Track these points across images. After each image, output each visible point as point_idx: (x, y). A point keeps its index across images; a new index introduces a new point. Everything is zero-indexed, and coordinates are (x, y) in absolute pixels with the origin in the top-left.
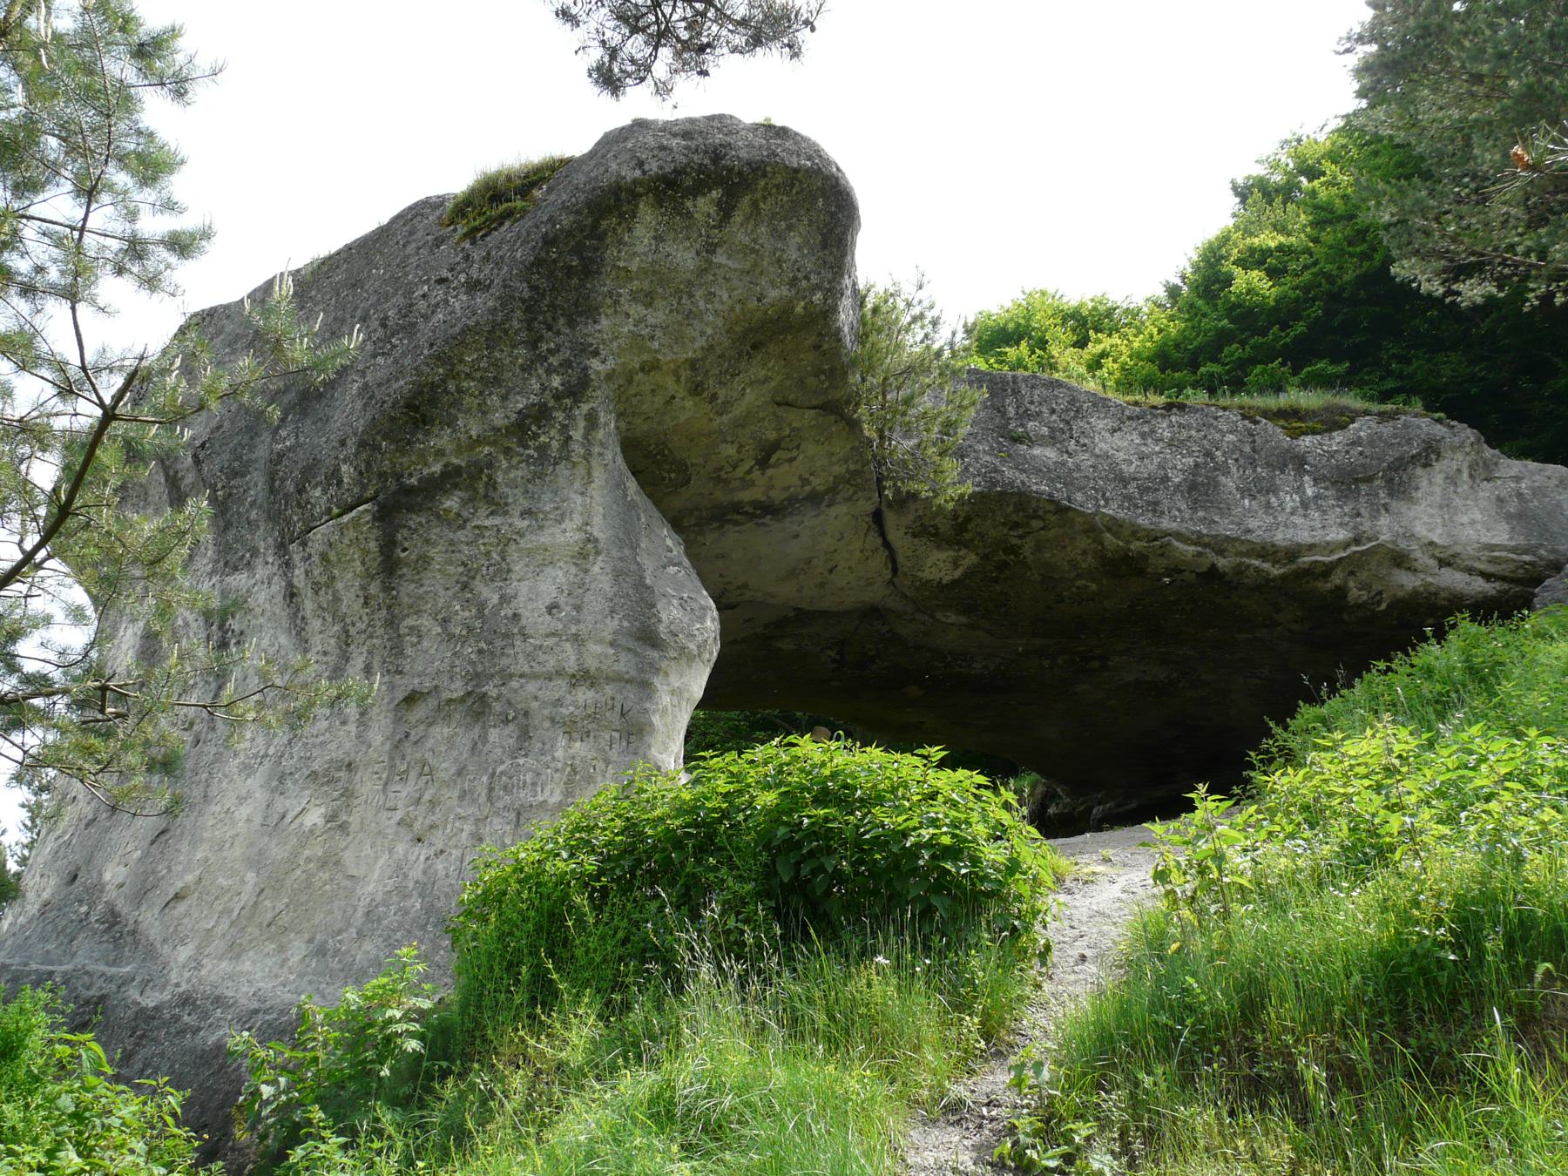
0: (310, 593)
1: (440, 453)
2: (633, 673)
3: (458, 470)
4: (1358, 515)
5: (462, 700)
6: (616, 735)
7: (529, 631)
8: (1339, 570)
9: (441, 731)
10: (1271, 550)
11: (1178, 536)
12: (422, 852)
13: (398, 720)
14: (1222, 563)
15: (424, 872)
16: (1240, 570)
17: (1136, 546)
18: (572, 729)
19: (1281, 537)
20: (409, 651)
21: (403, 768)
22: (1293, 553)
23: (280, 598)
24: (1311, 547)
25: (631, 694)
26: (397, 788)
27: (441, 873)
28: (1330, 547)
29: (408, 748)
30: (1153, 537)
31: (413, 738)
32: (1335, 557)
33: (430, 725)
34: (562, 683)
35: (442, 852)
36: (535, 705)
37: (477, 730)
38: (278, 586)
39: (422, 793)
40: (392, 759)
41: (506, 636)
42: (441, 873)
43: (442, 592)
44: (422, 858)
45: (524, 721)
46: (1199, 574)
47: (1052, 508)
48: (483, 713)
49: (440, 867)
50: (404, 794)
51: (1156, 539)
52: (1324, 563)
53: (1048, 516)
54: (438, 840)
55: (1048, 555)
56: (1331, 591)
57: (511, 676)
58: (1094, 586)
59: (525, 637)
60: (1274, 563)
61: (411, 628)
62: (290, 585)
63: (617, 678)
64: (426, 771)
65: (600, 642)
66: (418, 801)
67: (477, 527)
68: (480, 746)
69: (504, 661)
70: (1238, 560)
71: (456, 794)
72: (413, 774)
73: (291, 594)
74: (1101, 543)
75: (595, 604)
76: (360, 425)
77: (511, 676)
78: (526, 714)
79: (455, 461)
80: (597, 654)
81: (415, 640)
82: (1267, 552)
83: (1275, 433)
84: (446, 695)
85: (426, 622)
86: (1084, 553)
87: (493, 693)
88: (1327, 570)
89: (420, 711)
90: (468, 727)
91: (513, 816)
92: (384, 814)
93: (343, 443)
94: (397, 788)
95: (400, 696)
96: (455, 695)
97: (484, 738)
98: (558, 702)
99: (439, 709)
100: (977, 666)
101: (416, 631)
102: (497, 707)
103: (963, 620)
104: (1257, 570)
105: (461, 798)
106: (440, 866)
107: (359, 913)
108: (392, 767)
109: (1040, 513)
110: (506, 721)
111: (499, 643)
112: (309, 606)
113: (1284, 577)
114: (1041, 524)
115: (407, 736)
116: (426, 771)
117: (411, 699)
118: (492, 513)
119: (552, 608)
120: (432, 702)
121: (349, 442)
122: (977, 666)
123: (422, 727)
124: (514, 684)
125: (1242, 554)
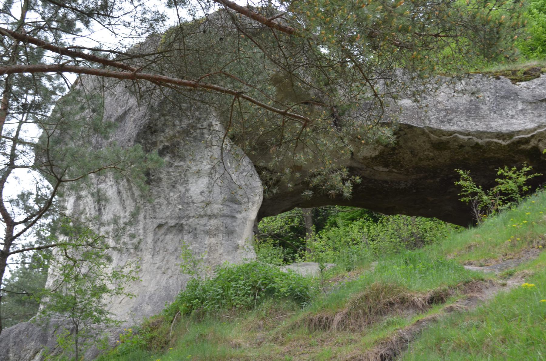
0: (125, 192)
1: (162, 142)
2: (229, 213)
3: (167, 147)
4: (540, 116)
5: (175, 226)
6: (224, 235)
7: (195, 201)
8: (533, 140)
9: (169, 237)
10: (501, 135)
11: (460, 133)
12: (166, 277)
13: (155, 234)
14: (480, 141)
15: (166, 283)
16: (489, 143)
17: (444, 138)
18: (208, 233)
19: (505, 129)
20: (157, 210)
21: (158, 250)
22: (511, 135)
23: (116, 193)
24: (519, 132)
25: (228, 221)
26: (156, 257)
27: (171, 283)
28: (526, 131)
29: (159, 243)
30: (451, 133)
31: (161, 240)
32: (529, 135)
33: (166, 235)
34: (206, 218)
35: (171, 277)
36: (198, 226)
37: (180, 236)
38: (115, 189)
39: (164, 257)
40: (154, 247)
41: (187, 203)
42: (171, 283)
43: (166, 189)
44: (165, 279)
45: (195, 232)
46: (472, 147)
47: (406, 127)
48: (182, 230)
49: (171, 281)
50: (158, 259)
51: (451, 135)
52: (525, 138)
53: (405, 130)
54: (170, 272)
55: (410, 144)
56: (531, 148)
57: (190, 217)
58: (432, 154)
59: (193, 203)
60: (504, 140)
61: (158, 203)
62: (118, 189)
63: (224, 216)
64: (166, 250)
65: (218, 204)
66: (163, 260)
67: (176, 166)
68: (181, 241)
69: (187, 212)
70: (488, 140)
71: (175, 257)
72: (161, 251)
73: (119, 192)
74: (429, 138)
75: (216, 190)
76: (134, 135)
77: (190, 217)
78: (196, 229)
79: (166, 144)
80: (216, 208)
81: (159, 206)
82: (500, 135)
83: (507, 82)
84: (170, 225)
85: (162, 200)
86: (424, 142)
87: (185, 223)
88: (527, 141)
89: (163, 230)
90: (178, 235)
91: (192, 264)
92: (153, 265)
93: (129, 140)
94: (156, 257)
95: (155, 226)
96: (173, 225)
97: (182, 238)
98: (205, 225)
99: (168, 229)
100: (402, 185)
101: (160, 204)
102: (186, 228)
103: (386, 169)
104: (496, 143)
105: (176, 259)
106: (171, 281)
107: (147, 297)
108: (155, 250)
109: (402, 129)
110: (189, 232)
111: (185, 206)
112: (125, 196)
113: (508, 145)
114: (404, 133)
115: (159, 239)
116: (166, 250)
117: (160, 226)
118: (181, 161)
119: (202, 193)
120: (166, 227)
121: (131, 140)
122: (402, 185)
123: (163, 236)
124: (191, 220)
125: (489, 138)
